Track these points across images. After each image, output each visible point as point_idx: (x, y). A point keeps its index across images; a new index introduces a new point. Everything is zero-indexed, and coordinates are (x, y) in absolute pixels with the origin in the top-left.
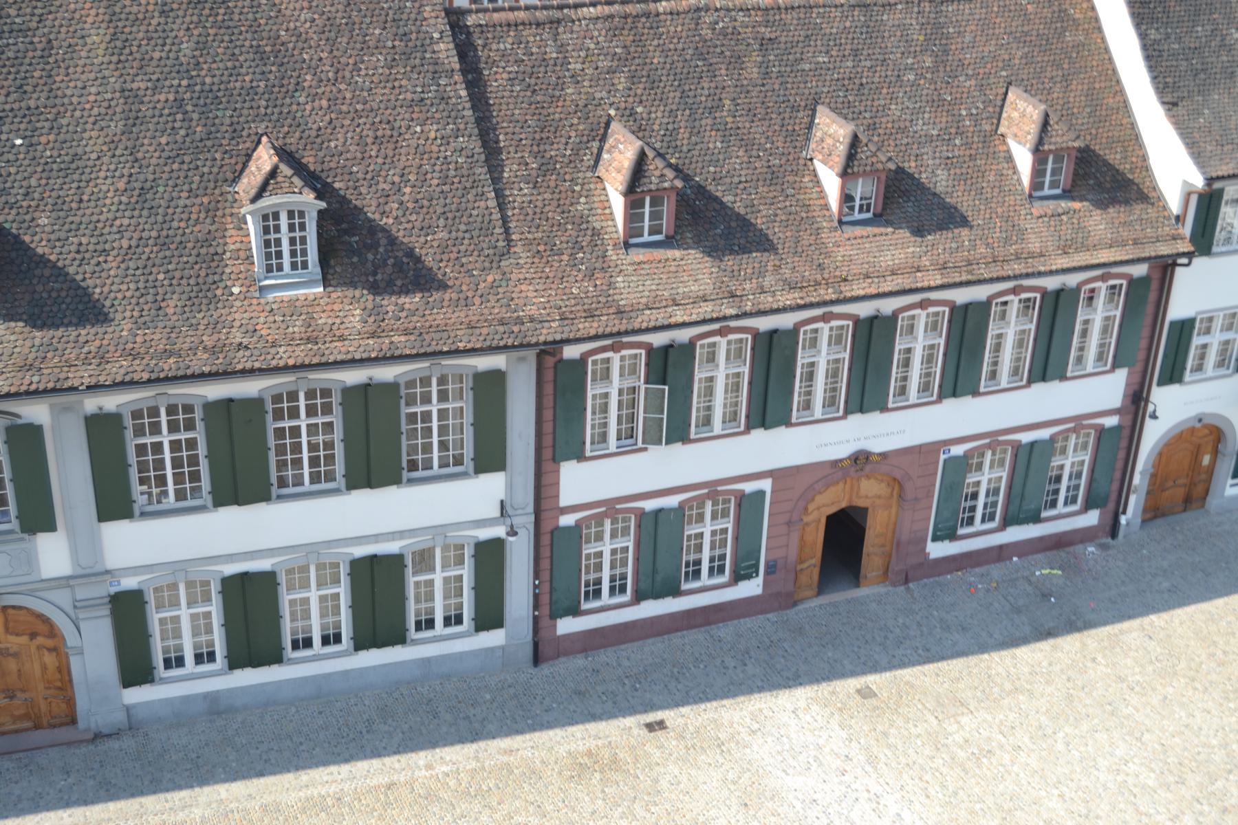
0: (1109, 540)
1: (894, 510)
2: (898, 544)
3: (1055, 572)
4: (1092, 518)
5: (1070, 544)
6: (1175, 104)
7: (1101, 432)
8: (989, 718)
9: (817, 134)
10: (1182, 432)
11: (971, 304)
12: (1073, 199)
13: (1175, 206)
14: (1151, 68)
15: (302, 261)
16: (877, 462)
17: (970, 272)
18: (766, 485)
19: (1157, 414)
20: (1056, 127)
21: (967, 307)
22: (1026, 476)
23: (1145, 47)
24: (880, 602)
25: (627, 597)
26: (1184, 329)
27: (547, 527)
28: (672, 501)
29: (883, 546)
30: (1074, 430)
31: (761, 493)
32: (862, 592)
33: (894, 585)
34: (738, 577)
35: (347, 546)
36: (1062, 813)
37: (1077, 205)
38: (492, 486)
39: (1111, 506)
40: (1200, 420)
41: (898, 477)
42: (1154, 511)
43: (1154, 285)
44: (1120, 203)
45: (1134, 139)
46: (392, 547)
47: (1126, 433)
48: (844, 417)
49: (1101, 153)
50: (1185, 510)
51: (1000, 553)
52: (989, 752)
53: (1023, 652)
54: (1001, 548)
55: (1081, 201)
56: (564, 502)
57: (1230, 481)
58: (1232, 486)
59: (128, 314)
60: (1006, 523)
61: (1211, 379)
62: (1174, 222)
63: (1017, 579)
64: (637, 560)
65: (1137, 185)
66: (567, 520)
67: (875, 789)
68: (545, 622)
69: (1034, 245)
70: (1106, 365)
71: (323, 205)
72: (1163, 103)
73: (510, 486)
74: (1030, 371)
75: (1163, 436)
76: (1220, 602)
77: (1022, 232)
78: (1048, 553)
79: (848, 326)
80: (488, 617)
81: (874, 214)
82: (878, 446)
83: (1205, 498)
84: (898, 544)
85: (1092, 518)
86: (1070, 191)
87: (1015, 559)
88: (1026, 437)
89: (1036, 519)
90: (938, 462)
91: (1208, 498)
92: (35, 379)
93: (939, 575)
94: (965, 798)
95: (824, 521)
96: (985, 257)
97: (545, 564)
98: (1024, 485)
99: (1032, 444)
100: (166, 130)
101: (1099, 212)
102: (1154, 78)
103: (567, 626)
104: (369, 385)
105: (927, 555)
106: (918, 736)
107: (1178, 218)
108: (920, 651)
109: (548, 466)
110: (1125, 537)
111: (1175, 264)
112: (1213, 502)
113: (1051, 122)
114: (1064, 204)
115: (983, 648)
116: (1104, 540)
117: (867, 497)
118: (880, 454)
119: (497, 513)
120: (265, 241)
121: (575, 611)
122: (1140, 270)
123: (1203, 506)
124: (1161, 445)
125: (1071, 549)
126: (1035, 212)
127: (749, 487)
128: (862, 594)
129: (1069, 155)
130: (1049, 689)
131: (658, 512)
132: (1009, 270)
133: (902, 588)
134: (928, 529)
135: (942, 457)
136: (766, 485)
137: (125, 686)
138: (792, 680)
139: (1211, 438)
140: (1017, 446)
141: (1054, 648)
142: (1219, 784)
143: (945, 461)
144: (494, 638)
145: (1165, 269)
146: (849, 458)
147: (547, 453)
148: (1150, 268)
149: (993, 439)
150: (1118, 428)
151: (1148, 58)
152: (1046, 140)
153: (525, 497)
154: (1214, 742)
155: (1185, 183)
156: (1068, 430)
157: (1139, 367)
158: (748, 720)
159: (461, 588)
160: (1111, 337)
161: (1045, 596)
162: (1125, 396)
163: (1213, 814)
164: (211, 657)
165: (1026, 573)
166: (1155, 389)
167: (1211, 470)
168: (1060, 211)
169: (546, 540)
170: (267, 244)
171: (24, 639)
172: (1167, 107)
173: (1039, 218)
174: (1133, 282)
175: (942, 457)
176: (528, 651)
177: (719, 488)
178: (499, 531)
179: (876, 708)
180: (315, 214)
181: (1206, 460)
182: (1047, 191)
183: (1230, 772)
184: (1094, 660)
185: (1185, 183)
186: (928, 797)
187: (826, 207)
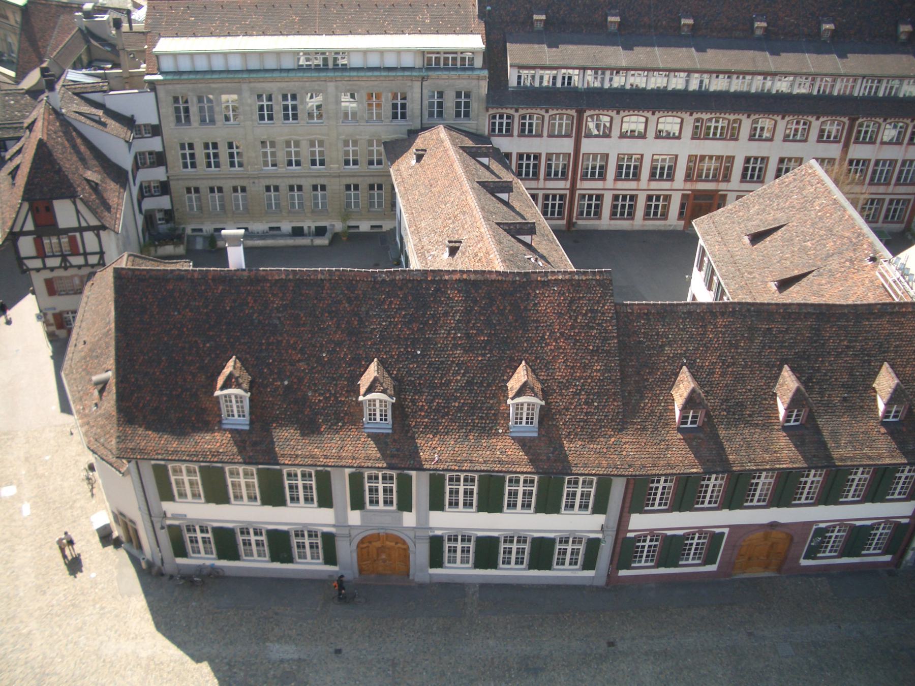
9: (781, 380)
18: (726, 530)
27: (621, 536)
28: (681, 532)
31: (723, 534)
32: (729, 207)
34: (705, 563)
38: (600, 519)
56: (630, 528)
59: (453, 436)
66: (630, 535)
71: (543, 403)
73: (607, 520)
82: (782, 520)
92: (412, 462)
119: (600, 529)
120: (457, 103)
121: (628, 567)
136: (726, 530)
137: (431, 568)
144: (591, 573)
147: (626, 510)
153: (614, 524)
170: (517, 414)
171: (393, 544)
175: (815, 527)
178: (600, 536)
180: (539, 407)
187: (777, 418)
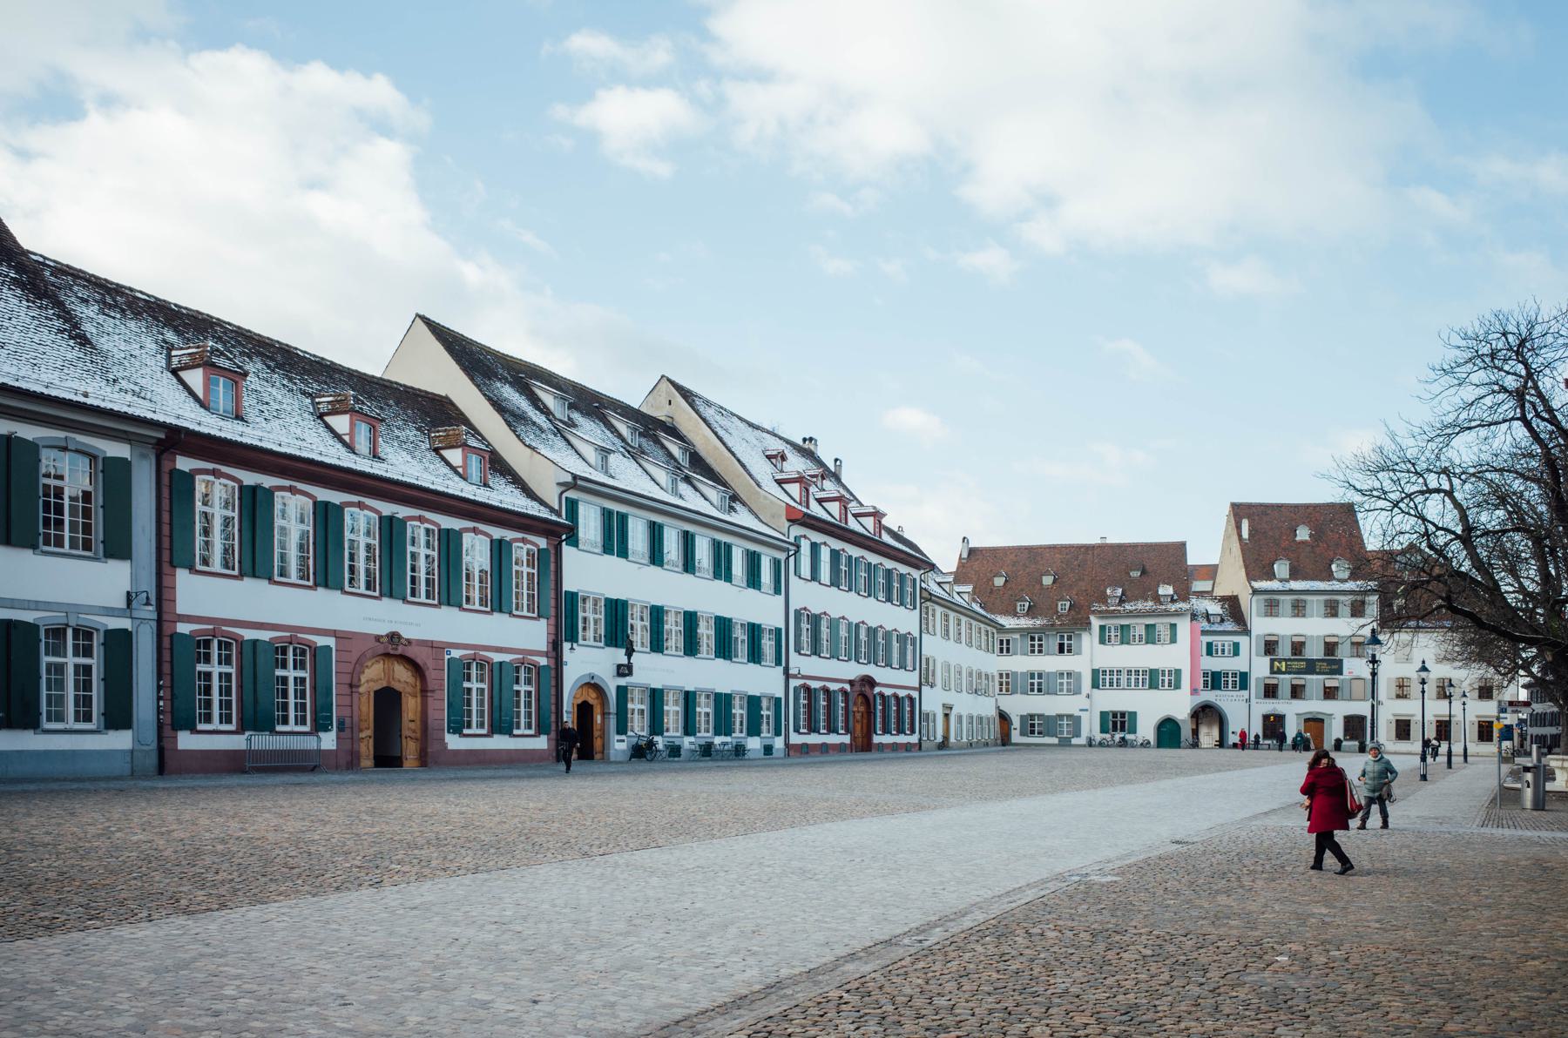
25: (232, 727)
27: (167, 630)
43: (553, 551)
46: (28, 617)
64: (240, 687)
68: (167, 731)
73: (134, 578)
80: (118, 717)
95: (372, 694)
97: (166, 668)
98: (255, 691)
100: (271, 880)
103: (186, 741)
105: (445, 745)
109: (166, 568)
119: (122, 604)
127: (321, 641)
131: (255, 642)
144: (121, 740)
146: (387, 635)
153: (148, 584)
159: (90, 681)
164: (1236, 646)
169: (166, 480)
175: (447, 657)
176: (153, 760)
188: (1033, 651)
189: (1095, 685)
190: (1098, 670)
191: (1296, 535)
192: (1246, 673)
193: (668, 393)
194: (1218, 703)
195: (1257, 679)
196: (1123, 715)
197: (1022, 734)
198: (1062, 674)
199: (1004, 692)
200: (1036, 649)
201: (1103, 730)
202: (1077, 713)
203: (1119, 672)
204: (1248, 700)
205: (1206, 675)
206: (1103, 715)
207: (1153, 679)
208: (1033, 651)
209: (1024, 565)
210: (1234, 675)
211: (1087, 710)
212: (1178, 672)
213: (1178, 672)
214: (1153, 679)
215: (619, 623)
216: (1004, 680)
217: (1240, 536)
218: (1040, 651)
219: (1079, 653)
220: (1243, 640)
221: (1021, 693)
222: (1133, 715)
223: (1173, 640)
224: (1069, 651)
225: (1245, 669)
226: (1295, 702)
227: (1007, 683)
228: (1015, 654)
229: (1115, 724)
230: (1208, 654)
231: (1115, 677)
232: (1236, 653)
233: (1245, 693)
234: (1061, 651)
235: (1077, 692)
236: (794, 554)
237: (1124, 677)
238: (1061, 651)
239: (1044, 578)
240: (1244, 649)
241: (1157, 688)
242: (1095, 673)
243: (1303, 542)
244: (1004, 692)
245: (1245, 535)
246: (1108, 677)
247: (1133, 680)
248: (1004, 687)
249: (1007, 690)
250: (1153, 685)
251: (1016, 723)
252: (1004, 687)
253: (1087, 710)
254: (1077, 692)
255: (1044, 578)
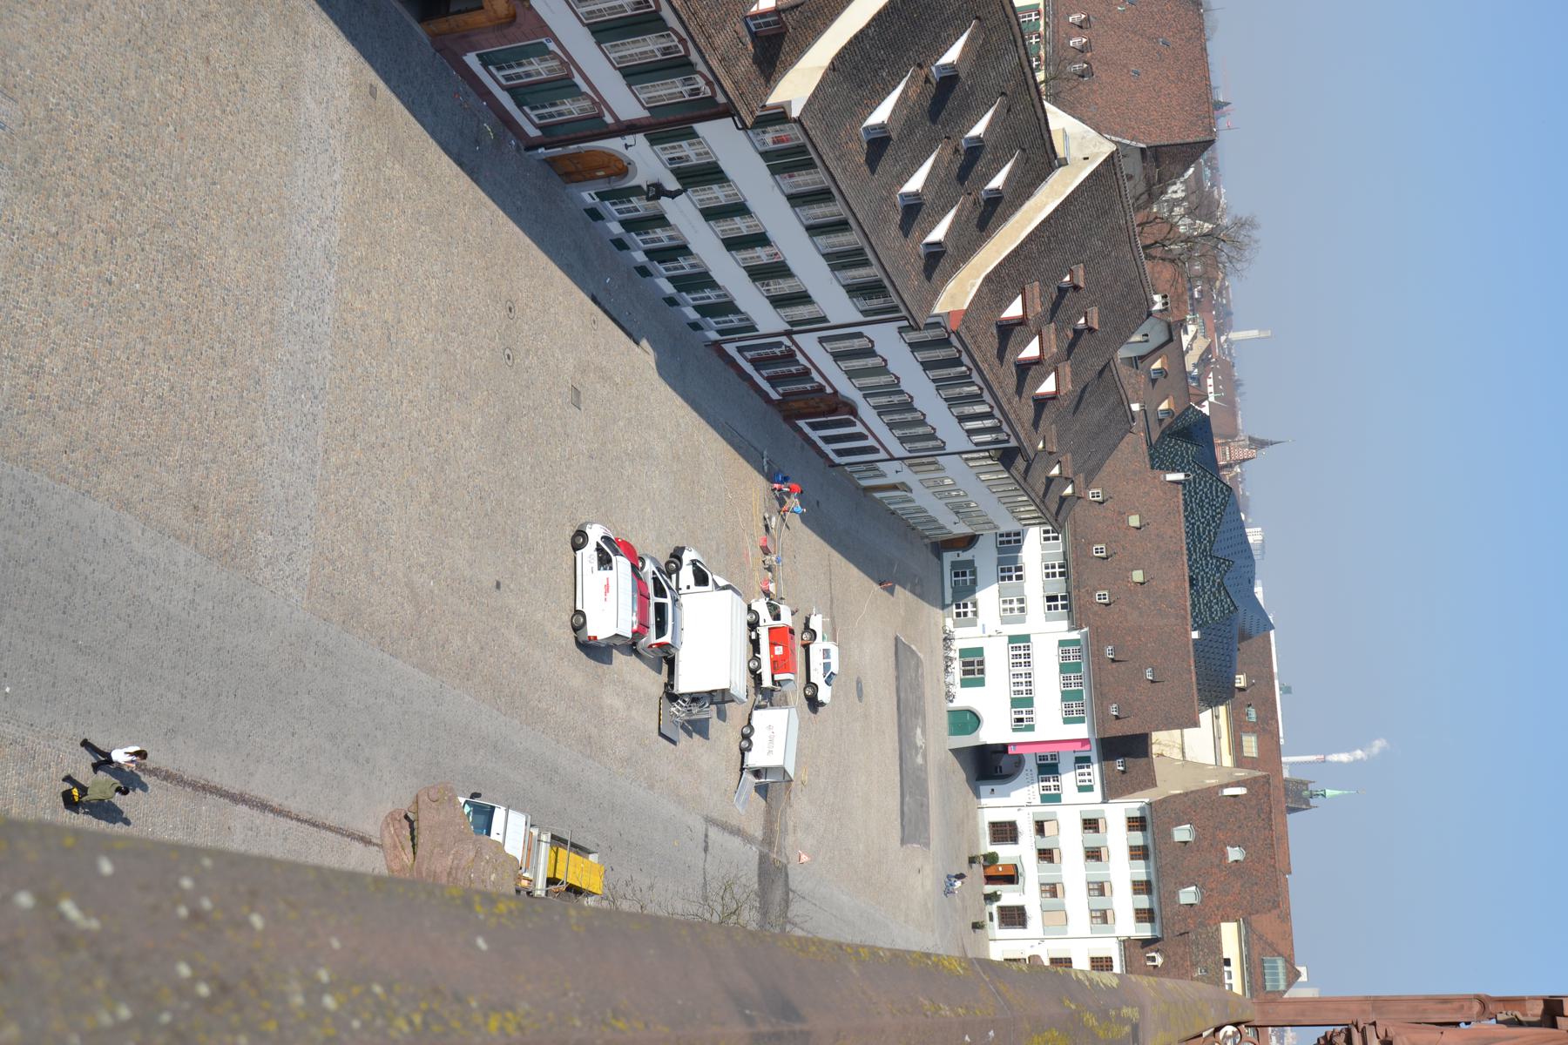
0: (523, 148)
1: (489, 24)
2: (464, 36)
3: (491, 134)
4: (533, 132)
5: (510, 129)
6: (834, 70)
7: (600, 116)
8: (406, 179)
10: (613, 156)
11: (664, 21)
12: (753, 41)
13: (773, 100)
14: (850, 42)
15: (1062, 600)
16: (524, 6)
17: (689, 18)
19: (629, 148)
20: (797, 13)
21: (661, 19)
22: (550, 90)
23: (862, 31)
24: (419, 45)
26: (694, 135)
29: (458, 26)
30: (594, 102)
32: (418, 28)
33: (433, 44)
35: (607, 109)
36: (393, 270)
37: (750, 47)
39: (548, 140)
40: (629, 164)
41: (518, 20)
42: (551, 162)
44: (760, 68)
45: (801, 50)
47: (605, 130)
48: (584, 25)
49: (786, 39)
50: (559, 175)
51: (486, 93)
52: (393, 198)
53: (445, 158)
54: (490, 93)
55: (754, 47)
57: (592, 193)
58: (590, 194)
60: (509, 90)
61: (691, 200)
62: (761, 105)
63: (475, 115)
65: (774, 70)
67: (338, 155)
69: (718, 41)
70: (647, 103)
72: (832, 63)
74: (596, 23)
75: (607, 148)
76: (528, 241)
77: (723, 28)
78: (498, 120)
79: (651, 7)
81: (756, 32)
83: (572, 182)
84: (464, 36)
85: (533, 132)
86: (757, 37)
87: (485, 103)
88: (578, 79)
89: (520, 105)
90: (538, 38)
91: (574, 184)
93: (453, 67)
94: (366, 210)
96: (700, 20)
99: (575, 85)
101: (751, 61)
102: (845, 48)
104: (692, 65)
106: (374, 149)
107: (764, 106)
108: (410, 100)
110: (529, 156)
111: (733, 116)
112: (573, 189)
113: (799, 9)
114: (748, 40)
115: (433, 135)
116: (521, 145)
117: (492, 5)
118: (530, 5)
122: (721, 99)
123: (567, 183)
124: (600, 149)
125: (507, 130)
126: (738, 28)
128: (416, 28)
129: (781, 27)
130: (438, 197)
132: (692, 27)
133: (433, 51)
134: (484, 49)
135: (544, 40)
138: (353, 37)
139: (617, 170)
140: (569, 77)
141: (457, 176)
142: (454, 334)
143: (542, 43)
145: (728, 111)
148: (725, 104)
149: (569, 62)
150: (607, 125)
151: (856, 37)
152: (787, 12)
154: (469, 311)
155: (790, 102)
156: (592, 99)
157: (653, 121)
158: (317, 33)
160: (609, 15)
161: (477, 142)
162: (630, 120)
163: (440, 346)
164: (1090, 789)
165: (481, 118)
166: (642, 134)
167: (594, 178)
168: (743, 40)
172: (831, 67)
173: (735, 31)
174: (712, 98)
175: (544, 40)
177: (572, 67)
179: (370, 107)
181: (601, 173)
182: (751, 24)
183: (462, 334)
184: (464, 205)
185: (790, 102)
186: (353, 189)
188: (1047, 568)
189: (1012, 639)
190: (1029, 641)
191: (1233, 847)
192: (1060, 801)
193: (1097, 155)
194: (1024, 772)
195: (1055, 813)
196: (982, 672)
197: (954, 565)
198: (1021, 601)
199: (1000, 539)
200: (1050, 571)
201: (963, 652)
202: (980, 621)
203: (1028, 664)
204: (1029, 805)
205: (1054, 757)
206: (979, 651)
207: (1022, 701)
208: (1047, 568)
209: (1159, 547)
210: (1057, 788)
211: (984, 632)
212: (1031, 728)
213: (1031, 728)
214: (1022, 701)
215: (701, 178)
216: (1013, 538)
217: (1227, 786)
218: (1047, 575)
219: (1047, 619)
220: (1097, 794)
221: (998, 558)
222: (981, 683)
223: (1066, 721)
224: (1049, 608)
225: (1064, 799)
226: (1034, 854)
227: (1009, 542)
228: (1043, 548)
229: (972, 664)
230: (1076, 758)
231: (1022, 660)
232: (1081, 789)
233: (1038, 801)
234: (1050, 599)
235: (1004, 621)
236: (911, 326)
237: (1022, 670)
238: (1050, 599)
239: (1141, 572)
240: (1086, 796)
241: (1013, 706)
242: (1026, 638)
243: (1225, 855)
244: (1000, 539)
245: (1228, 792)
246: (1022, 652)
247: (1019, 680)
248: (1005, 539)
249: (1001, 543)
250: (1015, 703)
251: (965, 556)
252: (1005, 539)
253: (984, 632)
254: (1004, 621)
255: (1141, 572)
